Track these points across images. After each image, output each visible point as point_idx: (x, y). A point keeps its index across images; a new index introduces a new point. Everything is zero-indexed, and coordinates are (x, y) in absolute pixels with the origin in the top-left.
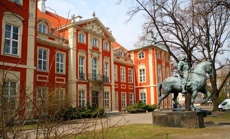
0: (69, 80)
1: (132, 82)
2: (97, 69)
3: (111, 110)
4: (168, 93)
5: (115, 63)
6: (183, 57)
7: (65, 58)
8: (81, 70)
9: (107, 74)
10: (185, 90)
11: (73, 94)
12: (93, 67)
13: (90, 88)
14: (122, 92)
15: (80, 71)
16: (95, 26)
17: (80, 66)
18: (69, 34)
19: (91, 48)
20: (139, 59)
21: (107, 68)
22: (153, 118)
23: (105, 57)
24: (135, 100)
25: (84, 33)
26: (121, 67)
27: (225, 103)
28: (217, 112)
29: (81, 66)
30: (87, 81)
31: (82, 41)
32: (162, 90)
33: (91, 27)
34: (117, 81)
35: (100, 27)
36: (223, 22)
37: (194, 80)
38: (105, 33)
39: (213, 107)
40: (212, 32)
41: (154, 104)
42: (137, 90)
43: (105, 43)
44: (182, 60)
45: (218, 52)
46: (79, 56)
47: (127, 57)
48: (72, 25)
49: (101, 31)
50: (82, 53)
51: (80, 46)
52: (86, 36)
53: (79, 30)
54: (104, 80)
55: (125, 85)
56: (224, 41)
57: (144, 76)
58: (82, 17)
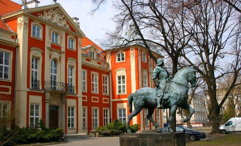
0: (16, 89)
1: (108, 93)
2: (57, 75)
3: (77, 133)
4: (140, 108)
5: (83, 67)
6: (160, 61)
7: (12, 58)
8: (34, 76)
9: (71, 81)
10: (161, 105)
11: (16, 110)
12: (52, 72)
13: (47, 101)
14: (92, 108)
15: (32, 77)
16: (56, 15)
17: (33, 70)
18: (18, 25)
19: (50, 46)
20: (117, 61)
21: (71, 73)
22: (120, 143)
23: (69, 59)
24: (112, 118)
25: (40, 25)
26: (92, 72)
27: (229, 122)
28: (217, 134)
29: (34, 70)
30: (43, 92)
31: (36, 36)
32: (133, 104)
33: (50, 17)
34: (87, 92)
35: (63, 16)
36: (224, 17)
37: (172, 91)
38: (69, 25)
39: (211, 128)
40: (212, 30)
41: (136, 123)
42: (115, 104)
43: (70, 38)
44: (159, 66)
45: (218, 55)
46: (33, 57)
47: (100, 58)
48: (23, 12)
49: (64, 23)
50: (36, 52)
51: (34, 43)
52: (42, 29)
53: (33, 21)
54: (67, 91)
55: (98, 98)
56: (227, 40)
57: (124, 85)
58: (39, 2)
